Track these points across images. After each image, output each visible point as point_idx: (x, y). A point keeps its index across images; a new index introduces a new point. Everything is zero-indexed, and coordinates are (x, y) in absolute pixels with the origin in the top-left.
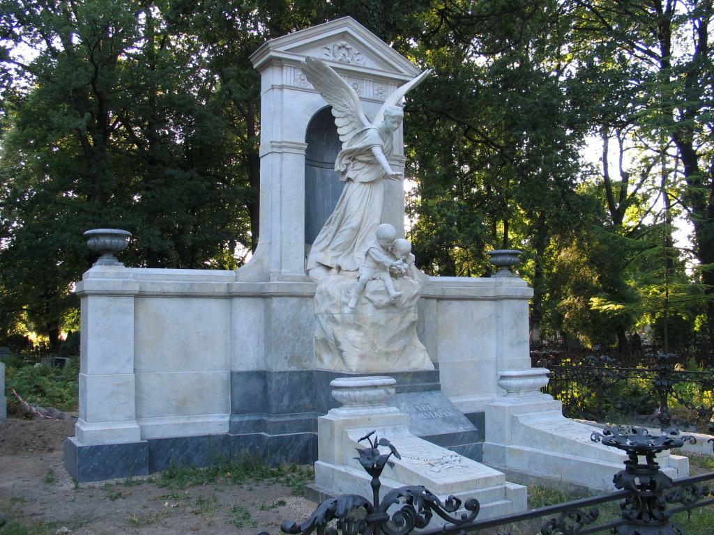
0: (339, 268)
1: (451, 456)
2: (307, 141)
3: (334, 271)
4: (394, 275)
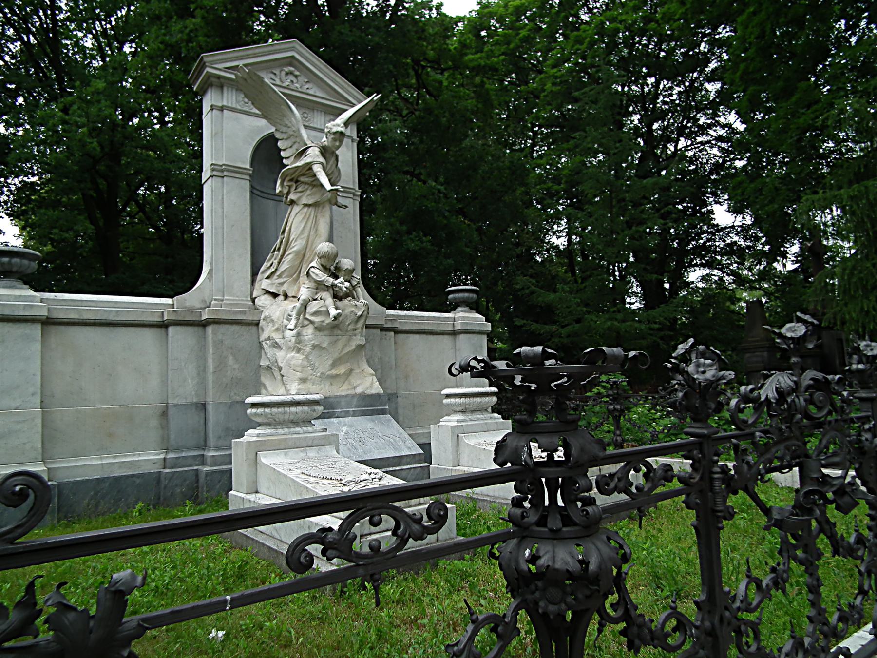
1: (370, 474)
2: (252, 166)
3: (281, 298)
4: (338, 297)
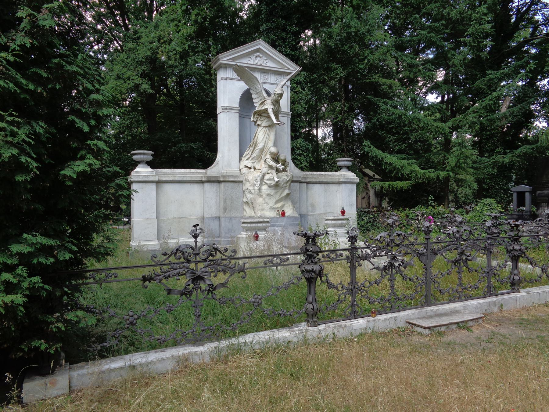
0: (255, 169)
3: (252, 170)
4: (278, 171)
